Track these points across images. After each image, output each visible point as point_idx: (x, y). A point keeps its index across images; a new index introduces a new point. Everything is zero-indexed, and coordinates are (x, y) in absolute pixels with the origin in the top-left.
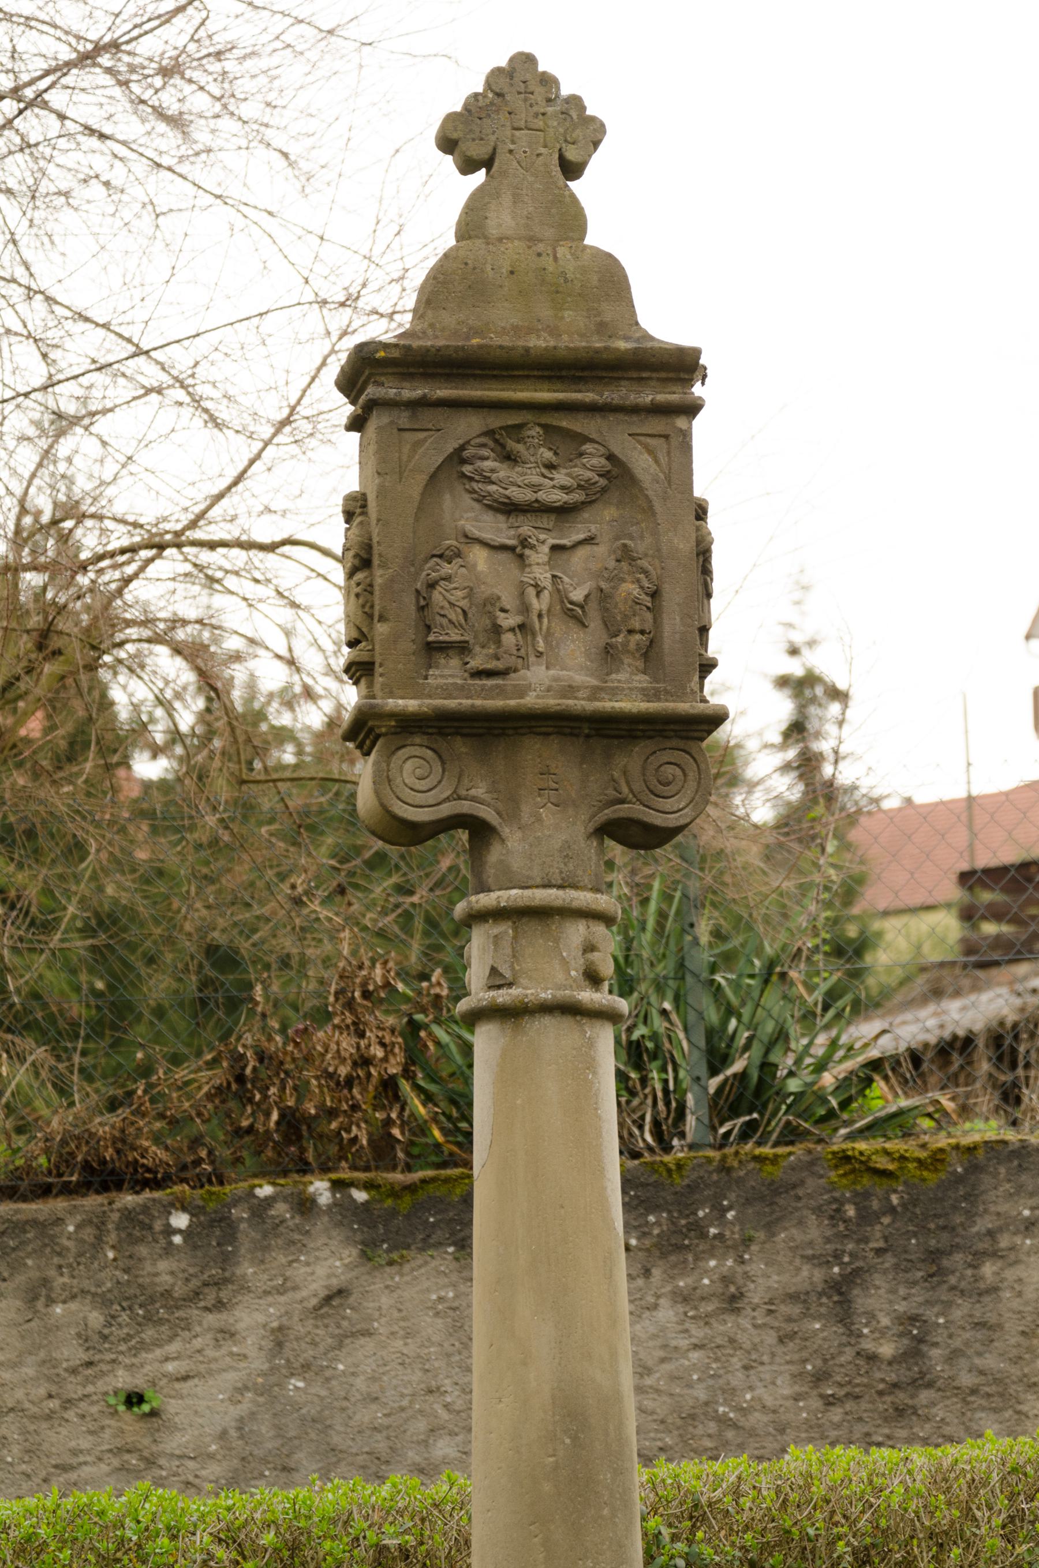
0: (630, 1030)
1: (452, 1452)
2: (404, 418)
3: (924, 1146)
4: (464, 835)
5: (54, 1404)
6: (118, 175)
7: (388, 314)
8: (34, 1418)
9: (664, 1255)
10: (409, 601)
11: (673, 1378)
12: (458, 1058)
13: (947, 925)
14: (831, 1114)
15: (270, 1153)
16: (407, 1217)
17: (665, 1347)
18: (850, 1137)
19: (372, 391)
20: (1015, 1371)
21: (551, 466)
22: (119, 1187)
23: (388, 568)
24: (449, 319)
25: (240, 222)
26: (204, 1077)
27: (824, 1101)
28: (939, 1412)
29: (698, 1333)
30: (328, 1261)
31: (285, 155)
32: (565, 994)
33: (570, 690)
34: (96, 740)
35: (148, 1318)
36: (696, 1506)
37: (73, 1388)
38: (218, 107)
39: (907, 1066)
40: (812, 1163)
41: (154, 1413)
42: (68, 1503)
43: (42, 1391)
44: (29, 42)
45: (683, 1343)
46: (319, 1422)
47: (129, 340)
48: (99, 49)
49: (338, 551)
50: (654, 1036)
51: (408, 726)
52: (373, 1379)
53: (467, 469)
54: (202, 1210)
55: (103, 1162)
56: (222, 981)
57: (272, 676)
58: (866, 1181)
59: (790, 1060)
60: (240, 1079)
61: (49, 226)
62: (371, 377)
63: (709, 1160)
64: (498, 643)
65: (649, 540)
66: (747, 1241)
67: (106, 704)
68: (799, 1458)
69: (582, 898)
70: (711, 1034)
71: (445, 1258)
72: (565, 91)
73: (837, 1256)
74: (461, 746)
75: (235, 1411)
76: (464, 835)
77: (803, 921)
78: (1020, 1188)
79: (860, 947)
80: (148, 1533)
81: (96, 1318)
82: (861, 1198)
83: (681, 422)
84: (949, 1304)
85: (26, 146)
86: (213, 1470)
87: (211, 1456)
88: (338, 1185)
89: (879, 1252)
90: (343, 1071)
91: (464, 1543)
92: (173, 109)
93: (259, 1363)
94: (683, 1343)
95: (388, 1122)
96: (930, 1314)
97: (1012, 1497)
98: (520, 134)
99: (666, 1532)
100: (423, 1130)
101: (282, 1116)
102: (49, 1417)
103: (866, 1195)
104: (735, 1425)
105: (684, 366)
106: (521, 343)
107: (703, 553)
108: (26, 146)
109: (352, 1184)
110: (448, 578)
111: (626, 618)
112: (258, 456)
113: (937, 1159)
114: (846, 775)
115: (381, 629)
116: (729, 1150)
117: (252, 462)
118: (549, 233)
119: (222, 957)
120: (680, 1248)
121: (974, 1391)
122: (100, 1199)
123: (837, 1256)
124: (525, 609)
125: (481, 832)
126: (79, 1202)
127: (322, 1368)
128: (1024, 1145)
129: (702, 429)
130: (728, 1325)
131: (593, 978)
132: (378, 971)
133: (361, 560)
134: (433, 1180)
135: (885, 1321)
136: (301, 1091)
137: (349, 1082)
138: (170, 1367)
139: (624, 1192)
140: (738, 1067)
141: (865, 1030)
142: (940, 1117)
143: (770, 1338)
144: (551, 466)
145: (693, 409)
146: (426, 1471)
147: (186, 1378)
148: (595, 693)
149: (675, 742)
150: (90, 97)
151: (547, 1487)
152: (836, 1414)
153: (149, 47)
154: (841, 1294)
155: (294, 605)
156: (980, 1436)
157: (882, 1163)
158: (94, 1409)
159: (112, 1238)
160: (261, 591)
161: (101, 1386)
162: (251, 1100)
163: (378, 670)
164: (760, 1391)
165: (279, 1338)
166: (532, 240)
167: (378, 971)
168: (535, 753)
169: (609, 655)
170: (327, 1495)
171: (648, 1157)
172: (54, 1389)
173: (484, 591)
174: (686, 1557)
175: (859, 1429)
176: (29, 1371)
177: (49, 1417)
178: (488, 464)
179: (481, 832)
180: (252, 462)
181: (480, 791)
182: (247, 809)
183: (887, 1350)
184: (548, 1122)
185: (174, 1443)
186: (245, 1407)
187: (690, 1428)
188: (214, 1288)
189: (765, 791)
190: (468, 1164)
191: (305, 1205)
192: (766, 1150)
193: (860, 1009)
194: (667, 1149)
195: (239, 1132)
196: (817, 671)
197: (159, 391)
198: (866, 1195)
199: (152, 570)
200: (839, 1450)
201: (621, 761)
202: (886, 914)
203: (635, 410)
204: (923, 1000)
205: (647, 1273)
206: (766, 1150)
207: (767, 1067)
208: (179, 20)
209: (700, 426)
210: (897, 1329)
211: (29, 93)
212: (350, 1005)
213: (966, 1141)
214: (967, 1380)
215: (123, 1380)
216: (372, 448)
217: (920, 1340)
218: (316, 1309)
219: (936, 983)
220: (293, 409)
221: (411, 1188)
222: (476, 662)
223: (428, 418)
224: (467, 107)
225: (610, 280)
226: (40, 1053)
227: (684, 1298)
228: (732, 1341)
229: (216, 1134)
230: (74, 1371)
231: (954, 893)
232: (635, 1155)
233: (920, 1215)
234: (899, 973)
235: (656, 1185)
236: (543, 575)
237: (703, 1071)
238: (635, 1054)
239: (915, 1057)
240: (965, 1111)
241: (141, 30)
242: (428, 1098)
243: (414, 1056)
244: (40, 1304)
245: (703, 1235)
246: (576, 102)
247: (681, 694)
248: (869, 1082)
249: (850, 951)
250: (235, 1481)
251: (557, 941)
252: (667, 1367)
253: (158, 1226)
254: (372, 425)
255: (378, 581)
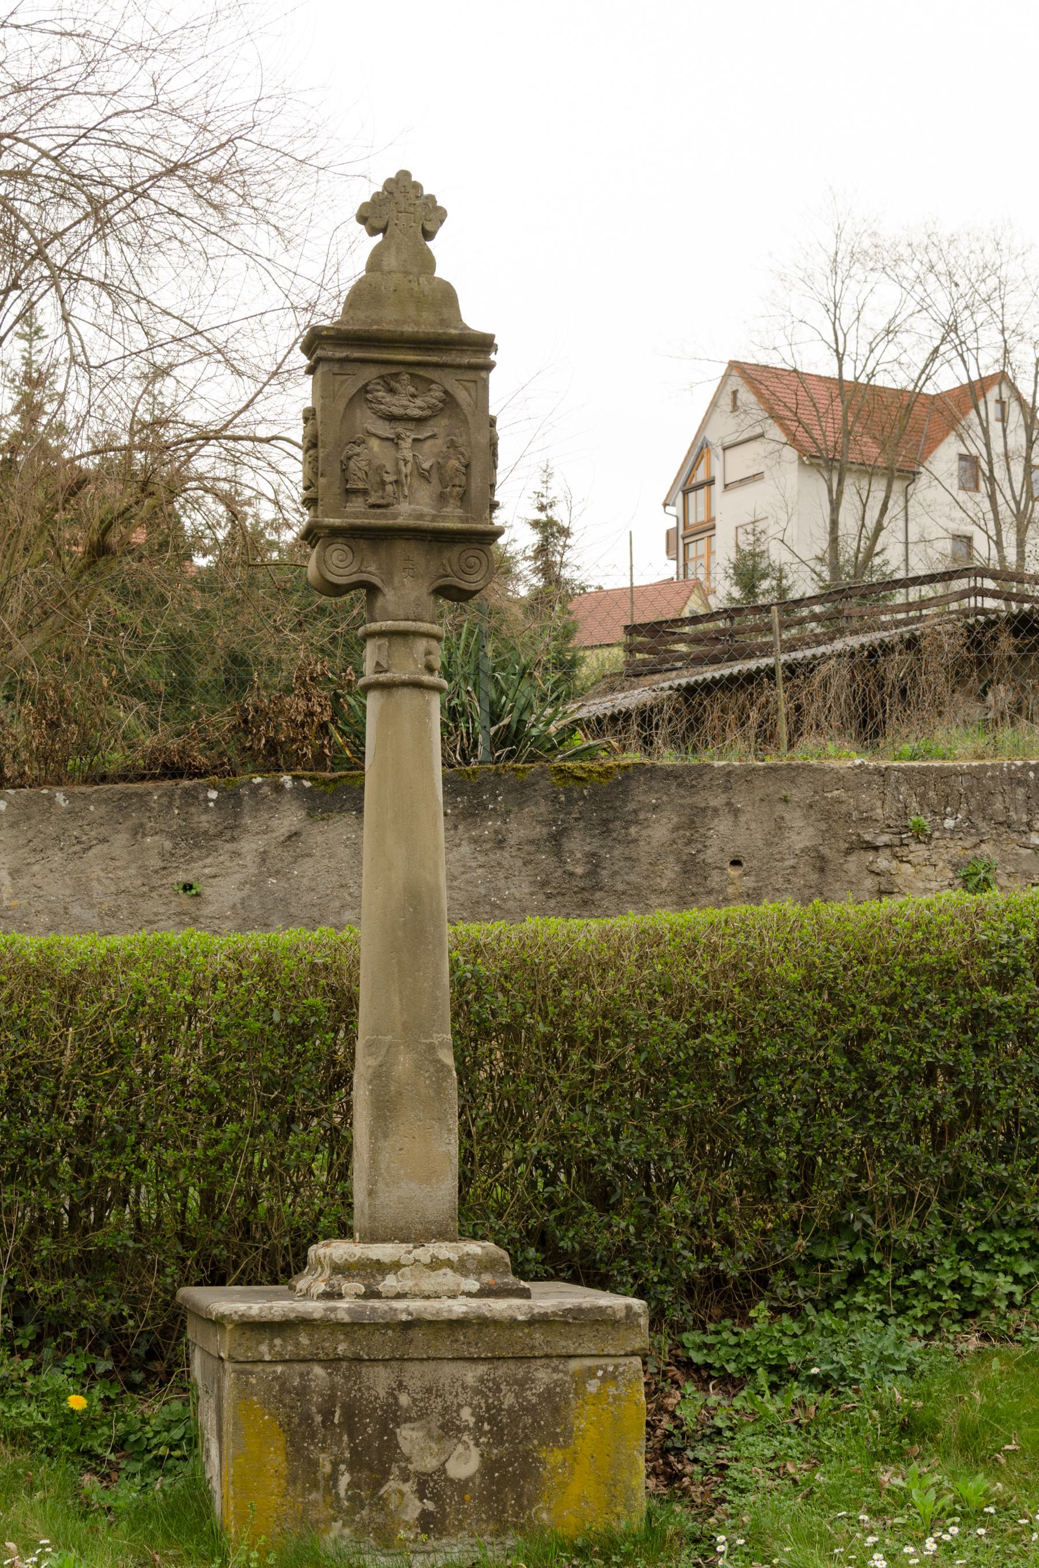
0: (450, 701)
1: (353, 918)
2: (336, 368)
3: (601, 765)
4: (364, 591)
5: (145, 889)
6: (187, 236)
7: (329, 312)
8: (134, 896)
9: (465, 819)
10: (337, 467)
11: (468, 882)
12: (360, 714)
13: (618, 653)
14: (554, 747)
15: (260, 760)
16: (332, 795)
17: (464, 866)
18: (562, 760)
19: (319, 353)
20: (645, 883)
21: (414, 396)
22: (181, 776)
23: (325, 446)
24: (361, 315)
25: (252, 263)
26: (225, 719)
27: (550, 740)
28: (605, 903)
29: (482, 859)
30: (290, 817)
31: (277, 229)
32: (415, 677)
33: (421, 516)
34: (174, 545)
35: (196, 845)
36: (478, 946)
37: (156, 881)
38: (241, 201)
39: (594, 725)
40: (543, 773)
41: (197, 895)
42: (151, 938)
43: (139, 882)
44: (139, 161)
45: (474, 864)
46: (284, 901)
47: (192, 326)
48: (176, 166)
49: (299, 440)
50: (463, 705)
51: (336, 533)
52: (313, 879)
53: (369, 396)
54: (224, 789)
55: (173, 763)
56: (237, 674)
57: (267, 512)
58: (571, 782)
59: (533, 717)
60: (246, 721)
61: (151, 263)
62: (315, 342)
63: (489, 770)
64: (384, 490)
65: (464, 437)
66: (508, 812)
67: (178, 525)
68: (532, 922)
69: (425, 627)
70: (492, 704)
71: (350, 818)
72: (426, 192)
73: (555, 821)
74: (363, 544)
75: (240, 894)
76: (364, 591)
77: (542, 646)
78: (651, 788)
79: (574, 663)
80: (192, 954)
81: (168, 845)
82: (568, 791)
83: (483, 374)
84: (612, 848)
85: (137, 219)
86: (228, 925)
87: (227, 918)
88: (295, 778)
89: (576, 819)
90: (299, 718)
91: (356, 962)
92: (217, 200)
93: (253, 870)
94: (474, 864)
95: (323, 746)
96: (602, 852)
97: (642, 945)
98: (402, 214)
99: (461, 959)
100: (341, 751)
101: (267, 741)
102: (143, 895)
103: (571, 790)
104: (500, 908)
105: (485, 344)
106: (399, 329)
107: (493, 445)
108: (137, 219)
109: (303, 778)
110: (358, 455)
111: (451, 478)
112: (260, 392)
113: (608, 772)
114: (566, 573)
115: (322, 481)
116: (500, 765)
117: (257, 395)
118: (415, 270)
119: (237, 660)
120: (473, 815)
121: (624, 893)
122: (171, 782)
123: (555, 821)
124: (398, 472)
125: (372, 590)
126: (160, 784)
127: (286, 873)
128: (654, 766)
129: (494, 378)
130: (498, 855)
131: (430, 669)
132: (319, 667)
133: (312, 444)
134: (346, 776)
135: (579, 855)
136: (277, 728)
137: (303, 724)
138: (207, 871)
139: (444, 784)
140: (506, 721)
141: (572, 706)
142: (610, 751)
143: (519, 863)
144: (414, 396)
145: (489, 367)
146: (339, 927)
147: (215, 877)
148: (434, 518)
149: (476, 546)
150: (172, 194)
151: (400, 934)
152: (552, 903)
153: (204, 166)
154: (556, 841)
155: (278, 472)
156: (626, 914)
157: (579, 773)
158: (167, 892)
159: (177, 803)
160: (261, 463)
161: (170, 880)
162: (251, 733)
163: (320, 503)
164: (513, 890)
165: (264, 857)
166: (406, 273)
167: (319, 667)
168: (401, 549)
169: (442, 498)
170: (286, 937)
171: (458, 767)
172: (146, 881)
173: (377, 462)
174: (472, 972)
175: (564, 911)
176: (133, 871)
177: (143, 895)
178: (380, 394)
179: (372, 590)
180: (257, 395)
181: (373, 568)
182: (252, 582)
183: (579, 870)
184: (405, 744)
185: (208, 910)
186: (245, 892)
187: (475, 908)
188: (231, 830)
189: (526, 583)
190: (363, 769)
191: (279, 788)
192: (519, 765)
193: (569, 696)
194: (468, 763)
195: (244, 749)
196: (555, 518)
197: (209, 354)
198: (571, 790)
199: (202, 452)
200: (552, 919)
201: (447, 554)
202: (586, 648)
203: (459, 367)
204: (605, 693)
205: (456, 827)
206: (519, 765)
207: (521, 722)
208: (221, 152)
209: (494, 377)
210: (585, 860)
211: (139, 189)
212: (304, 684)
213: (623, 763)
214: (620, 887)
215: (182, 877)
216: (319, 383)
217: (597, 866)
218: (284, 842)
219: (612, 683)
220: (279, 367)
221: (334, 781)
222: (372, 500)
223: (349, 368)
224: (373, 199)
225: (447, 296)
226: (141, 706)
227: (475, 841)
228: (499, 864)
229: (232, 752)
230: (156, 872)
231: (621, 636)
232: (451, 766)
233: (600, 801)
234: (593, 679)
235: (462, 782)
236: (408, 454)
237: (487, 723)
238: (453, 714)
239: (599, 721)
240: (624, 749)
241: (200, 157)
242: (343, 733)
243: (336, 713)
244: (139, 837)
245: (486, 809)
246: (432, 198)
247: (480, 520)
248: (574, 731)
249: (567, 667)
250: (240, 929)
251: (411, 649)
252: (465, 876)
253: (201, 797)
254: (319, 371)
255: (321, 455)
